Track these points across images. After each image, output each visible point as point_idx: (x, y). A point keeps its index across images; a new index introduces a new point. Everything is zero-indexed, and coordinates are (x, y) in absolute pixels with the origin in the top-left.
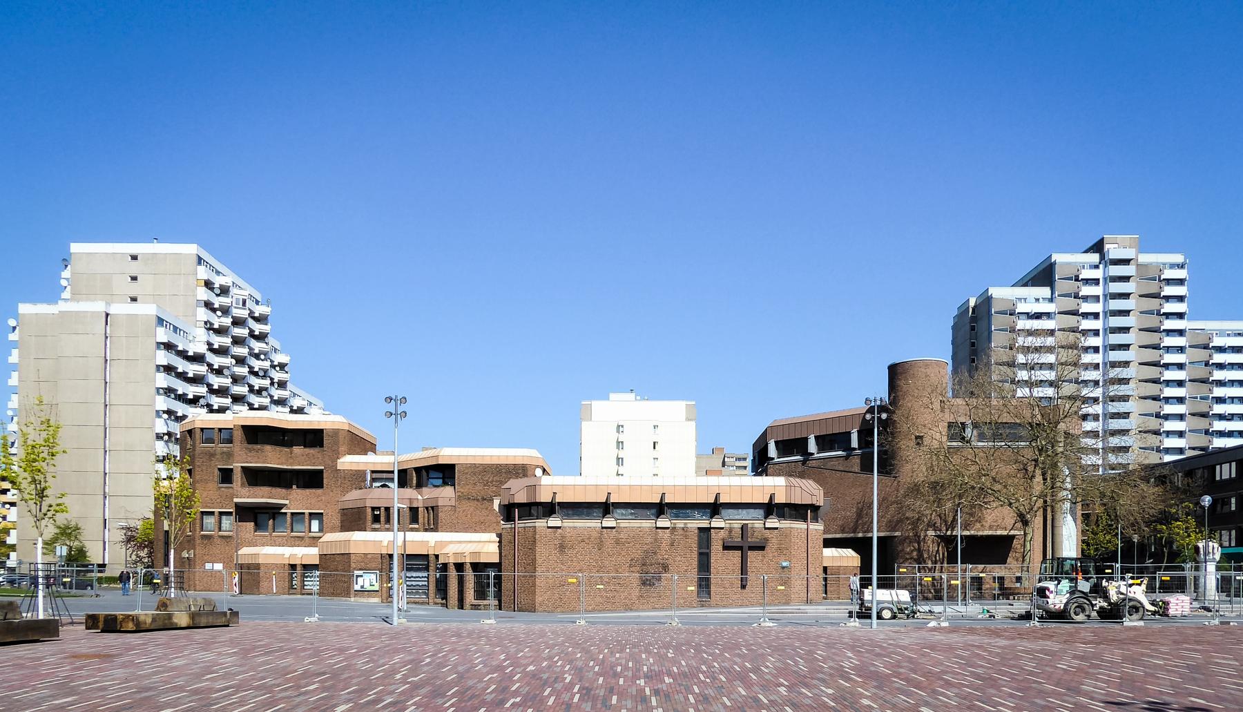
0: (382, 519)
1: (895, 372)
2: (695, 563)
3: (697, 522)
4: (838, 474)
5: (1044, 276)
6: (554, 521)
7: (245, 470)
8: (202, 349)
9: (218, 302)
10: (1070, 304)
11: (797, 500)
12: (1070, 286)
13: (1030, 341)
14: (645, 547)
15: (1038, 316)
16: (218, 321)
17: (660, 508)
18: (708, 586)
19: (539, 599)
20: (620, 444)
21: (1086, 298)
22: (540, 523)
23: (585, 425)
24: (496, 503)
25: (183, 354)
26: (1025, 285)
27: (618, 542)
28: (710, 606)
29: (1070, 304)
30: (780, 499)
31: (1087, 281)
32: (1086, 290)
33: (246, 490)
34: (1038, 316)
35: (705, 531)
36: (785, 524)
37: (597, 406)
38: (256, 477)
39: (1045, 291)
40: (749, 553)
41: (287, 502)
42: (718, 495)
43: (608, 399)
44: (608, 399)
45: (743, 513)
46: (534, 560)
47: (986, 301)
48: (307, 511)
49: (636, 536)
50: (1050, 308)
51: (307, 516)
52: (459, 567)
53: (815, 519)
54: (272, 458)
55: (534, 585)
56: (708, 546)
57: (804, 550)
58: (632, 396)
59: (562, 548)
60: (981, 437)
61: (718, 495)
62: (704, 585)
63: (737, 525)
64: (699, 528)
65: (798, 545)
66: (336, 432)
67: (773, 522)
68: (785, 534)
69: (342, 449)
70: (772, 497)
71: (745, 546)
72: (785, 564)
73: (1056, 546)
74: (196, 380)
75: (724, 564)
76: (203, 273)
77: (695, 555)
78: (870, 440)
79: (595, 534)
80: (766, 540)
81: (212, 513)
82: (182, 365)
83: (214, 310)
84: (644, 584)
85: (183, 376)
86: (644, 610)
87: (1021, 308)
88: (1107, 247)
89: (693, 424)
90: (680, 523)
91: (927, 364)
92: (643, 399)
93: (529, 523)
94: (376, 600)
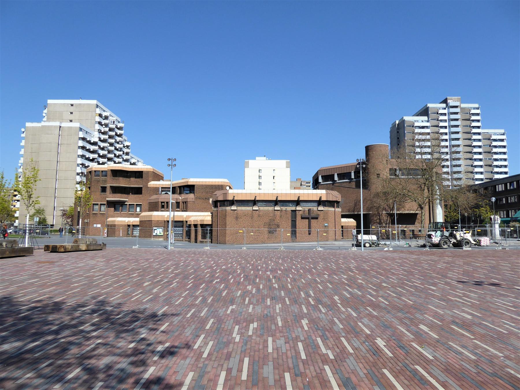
0: (165, 206)
2: (290, 224)
5: (425, 112)
6: (234, 208)
9: (104, 122)
10: (435, 123)
13: (420, 137)
14: (270, 218)
15: (423, 127)
16: (103, 129)
17: (276, 202)
18: (295, 234)
19: (227, 239)
20: (260, 177)
22: (228, 208)
24: (211, 200)
25: (89, 142)
27: (259, 216)
29: (435, 123)
30: (324, 199)
32: (441, 118)
33: (111, 195)
34: (423, 127)
37: (251, 162)
38: (116, 190)
39: (426, 118)
40: (312, 220)
41: (127, 200)
42: (299, 197)
43: (255, 159)
44: (255, 159)
45: (309, 204)
46: (226, 223)
47: (403, 122)
48: (135, 203)
50: (428, 124)
52: (196, 226)
53: (338, 207)
56: (296, 217)
59: (237, 218)
60: (403, 174)
61: (299, 197)
62: (294, 233)
63: (307, 209)
65: (331, 218)
67: (321, 208)
68: (327, 212)
69: (150, 179)
71: (310, 217)
72: (326, 225)
74: (94, 152)
75: (302, 225)
77: (290, 221)
78: (359, 175)
79: (250, 213)
81: (98, 204)
82: (88, 146)
83: (102, 125)
85: (89, 151)
87: (416, 124)
88: (449, 101)
90: (284, 208)
91: (380, 146)
94: (161, 239)
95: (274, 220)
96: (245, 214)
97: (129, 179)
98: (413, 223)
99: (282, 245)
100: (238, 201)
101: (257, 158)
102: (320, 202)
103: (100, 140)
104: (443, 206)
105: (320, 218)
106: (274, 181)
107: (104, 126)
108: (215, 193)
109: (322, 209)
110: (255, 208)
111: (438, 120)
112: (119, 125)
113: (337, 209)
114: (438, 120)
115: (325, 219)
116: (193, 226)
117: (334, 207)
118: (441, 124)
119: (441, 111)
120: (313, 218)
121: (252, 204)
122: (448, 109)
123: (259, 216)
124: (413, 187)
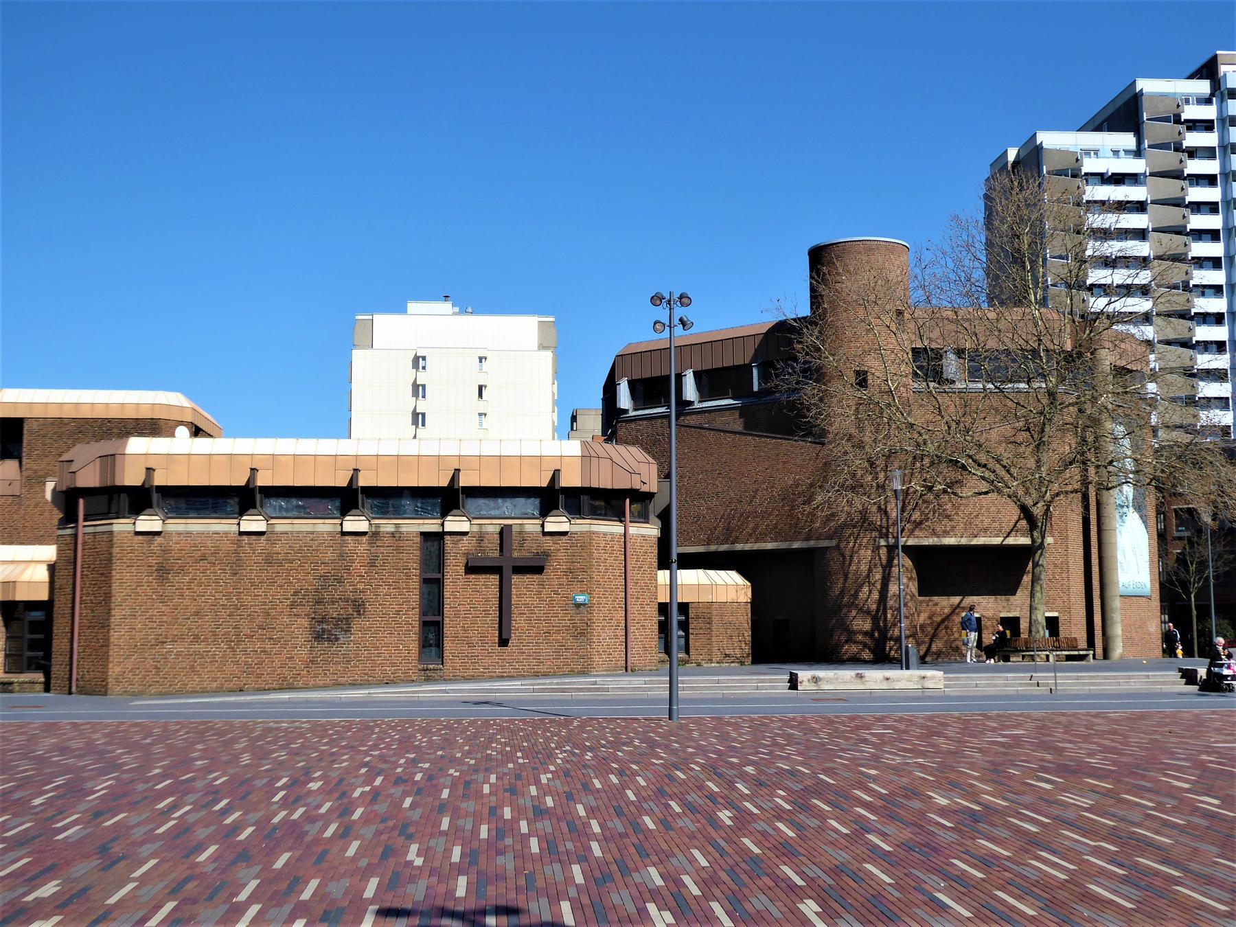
1: (819, 257)
3: (415, 526)
4: (730, 438)
5: (1125, 114)
6: (148, 523)
10: (1168, 159)
11: (606, 483)
12: (1164, 131)
13: (1109, 220)
14: (322, 570)
15: (1118, 179)
17: (347, 498)
18: (439, 644)
19: (114, 670)
20: (418, 390)
21: (1192, 153)
22: (121, 526)
23: (358, 356)
24: (50, 486)
26: (1098, 129)
27: (269, 560)
28: (445, 680)
29: (1168, 159)
30: (571, 479)
31: (1193, 125)
32: (1193, 139)
34: (1118, 179)
35: (434, 539)
36: (582, 525)
37: (385, 325)
39: (1127, 140)
40: (516, 579)
42: (556, 474)
43: (403, 311)
44: (403, 311)
45: (506, 505)
46: (108, 596)
47: (1033, 156)
49: (305, 548)
50: (1137, 166)
53: (643, 517)
55: (106, 644)
56: (441, 566)
57: (619, 572)
58: (447, 307)
59: (163, 572)
60: (974, 374)
61: (556, 474)
62: (432, 634)
63: (492, 527)
64: (422, 533)
65: (606, 569)
67: (557, 523)
68: (585, 543)
71: (506, 565)
72: (580, 598)
73: (1106, 563)
75: (468, 600)
77: (415, 583)
78: (771, 382)
79: (227, 546)
86: (317, 688)
87: (1090, 165)
88: (1223, 69)
89: (548, 355)
90: (387, 525)
91: (870, 248)
92: (464, 312)
93: (100, 526)
96: (204, 554)
98: (1010, 588)
100: (170, 492)
101: (412, 307)
104: (1152, 513)
105: (555, 568)
106: (481, 406)
108: (66, 457)
109: (565, 527)
110: (253, 523)
111: (1178, 148)
113: (635, 530)
114: (1178, 148)
115: (578, 573)
117: (619, 516)
118: (1195, 166)
119: (1192, 112)
120: (520, 570)
122: (1222, 100)
123: (269, 560)
124: (995, 434)
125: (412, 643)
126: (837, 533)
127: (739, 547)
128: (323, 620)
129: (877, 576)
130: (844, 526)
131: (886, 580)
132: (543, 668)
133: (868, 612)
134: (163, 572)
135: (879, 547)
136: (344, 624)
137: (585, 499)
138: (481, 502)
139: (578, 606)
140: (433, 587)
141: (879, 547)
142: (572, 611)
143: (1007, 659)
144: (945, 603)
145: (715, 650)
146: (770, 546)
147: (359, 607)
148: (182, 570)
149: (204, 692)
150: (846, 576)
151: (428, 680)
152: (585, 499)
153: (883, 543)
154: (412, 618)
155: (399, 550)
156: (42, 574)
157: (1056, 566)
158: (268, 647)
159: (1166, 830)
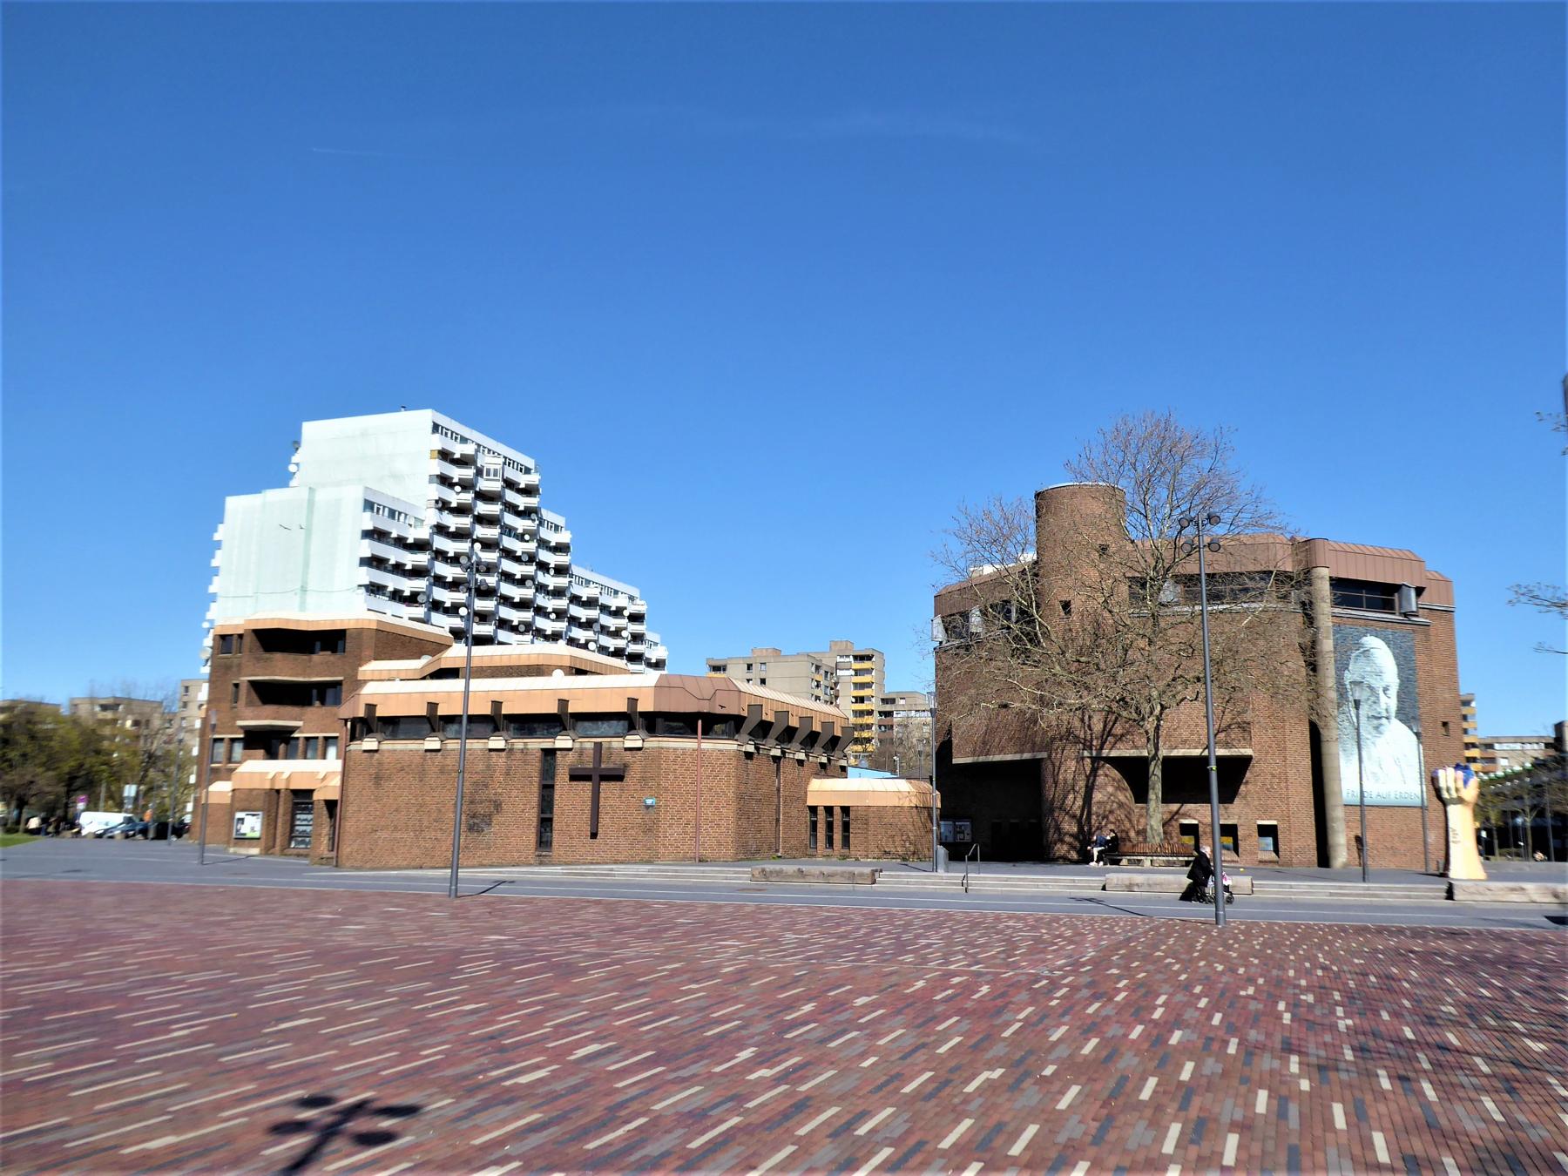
3: (537, 744)
7: (253, 684)
8: (423, 533)
9: (457, 473)
16: (455, 497)
25: (401, 542)
30: (646, 706)
33: (248, 711)
38: (270, 693)
40: (604, 785)
41: (300, 724)
45: (604, 726)
51: (320, 742)
52: (829, 810)
54: (285, 669)
59: (378, 779)
63: (589, 744)
66: (360, 631)
67: (633, 741)
69: (368, 653)
70: (633, 702)
72: (649, 802)
74: (417, 572)
75: (571, 799)
76: (438, 442)
79: (417, 760)
80: (626, 766)
81: (221, 740)
82: (394, 555)
83: (451, 485)
84: (471, 829)
85: (398, 569)
90: (519, 744)
94: (255, 851)
95: (486, 786)
97: (305, 657)
99: (509, 869)
100: (512, 718)
102: (631, 719)
103: (441, 529)
107: (458, 488)
112: (523, 480)
116: (821, 812)
121: (620, 726)
125: (532, 837)
126: (1048, 747)
127: (991, 758)
128: (474, 816)
129: (1082, 784)
130: (1053, 739)
131: (1089, 790)
132: (621, 857)
133: (1074, 816)
134: (378, 779)
135: (1083, 758)
136: (488, 819)
137: (659, 721)
138: (587, 724)
139: (648, 807)
140: (547, 790)
141: (1083, 758)
142: (643, 811)
143: (1117, 862)
144: (1175, 807)
145: (872, 847)
146: (1009, 757)
147: (498, 806)
148: (389, 778)
149: (399, 868)
150: (1056, 783)
151: (541, 864)
152: (659, 721)
153: (1086, 753)
154: (532, 815)
155: (525, 762)
156: (337, 781)
157: (1273, 776)
158: (439, 835)
159: (884, 1027)
